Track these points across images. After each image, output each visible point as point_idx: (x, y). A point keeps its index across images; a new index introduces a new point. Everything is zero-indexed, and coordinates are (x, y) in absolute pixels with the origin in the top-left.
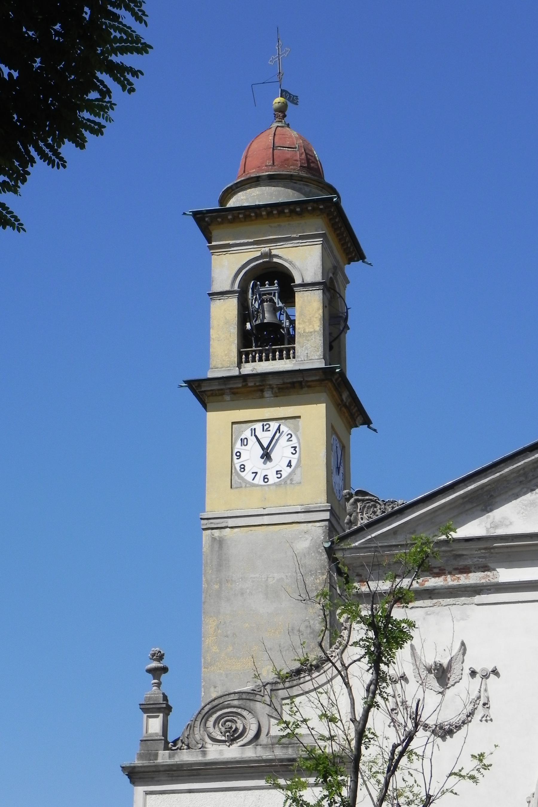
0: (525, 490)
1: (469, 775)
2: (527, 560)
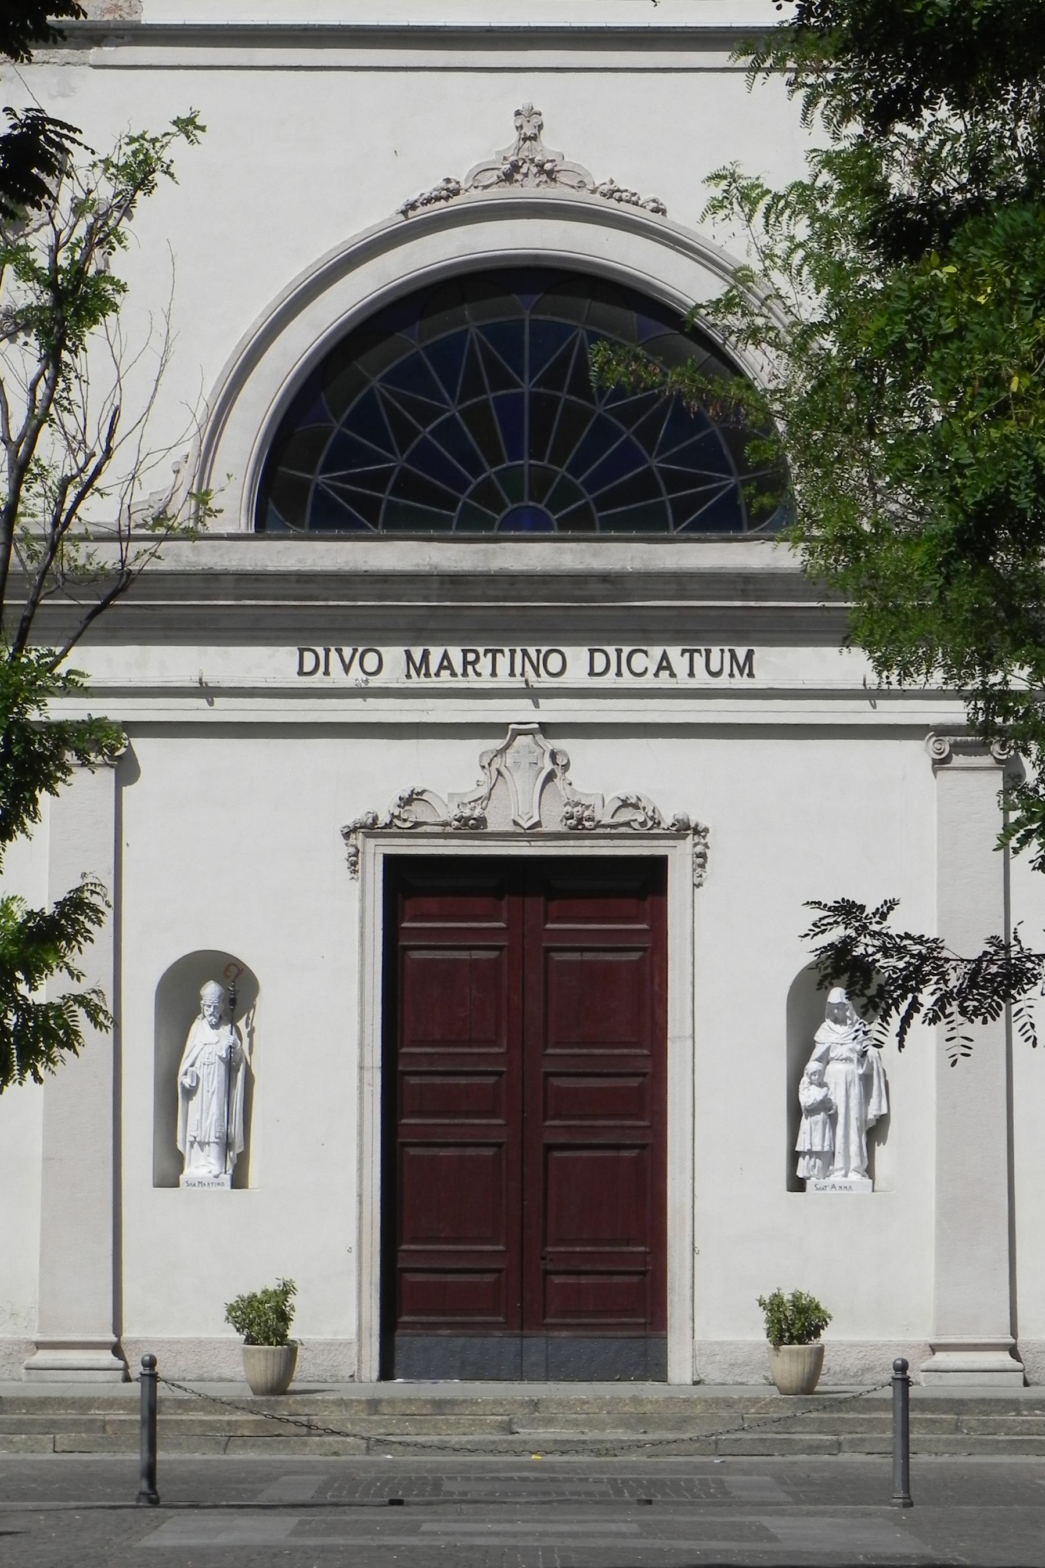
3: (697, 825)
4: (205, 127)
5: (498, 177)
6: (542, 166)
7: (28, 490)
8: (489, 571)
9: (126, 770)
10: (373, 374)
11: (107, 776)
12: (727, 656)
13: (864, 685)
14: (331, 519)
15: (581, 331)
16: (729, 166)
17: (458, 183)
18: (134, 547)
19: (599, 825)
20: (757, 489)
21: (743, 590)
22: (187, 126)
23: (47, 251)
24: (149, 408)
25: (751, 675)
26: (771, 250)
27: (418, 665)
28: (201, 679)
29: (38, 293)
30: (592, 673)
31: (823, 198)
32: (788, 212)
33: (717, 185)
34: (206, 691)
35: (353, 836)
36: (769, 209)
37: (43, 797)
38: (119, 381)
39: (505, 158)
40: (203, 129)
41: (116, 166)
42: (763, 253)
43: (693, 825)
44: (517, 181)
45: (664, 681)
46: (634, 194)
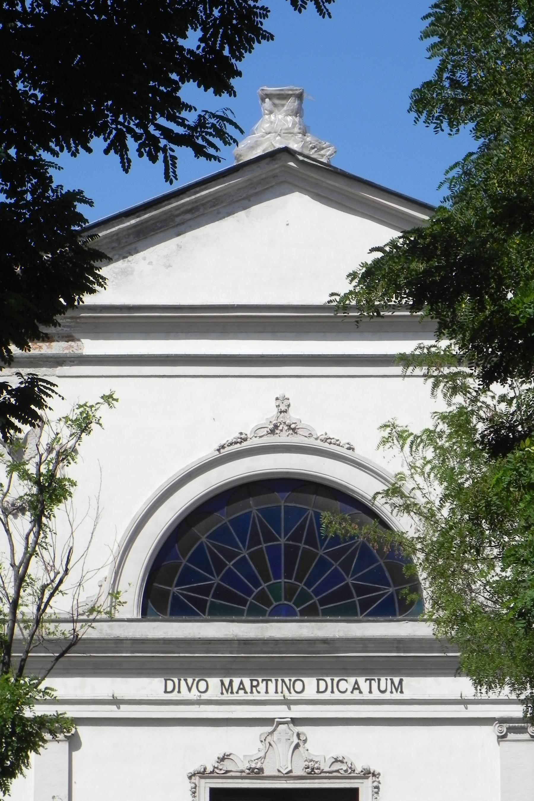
0: (117, 256)
1: (105, 611)
2: (115, 333)
3: (374, 772)
4: (118, 399)
5: (267, 432)
6: (290, 426)
7: (24, 591)
8: (264, 638)
9: (74, 743)
10: (203, 535)
11: (65, 746)
12: (389, 682)
13: (461, 697)
14: (181, 611)
15: (311, 511)
16: (391, 420)
17: (246, 435)
18: (79, 625)
19: (322, 772)
20: (410, 590)
21: (397, 647)
22: (109, 399)
23: (35, 465)
24: (88, 548)
25: (402, 692)
26: (414, 464)
27: (227, 687)
28: (113, 695)
29: (30, 487)
30: (318, 692)
31: (440, 437)
32: (422, 445)
33: (384, 431)
34: (116, 702)
35: (193, 778)
36: (412, 443)
37: (32, 755)
38: (72, 533)
39: (271, 422)
40: (117, 400)
41: (71, 420)
42: (410, 465)
43: (372, 771)
44: (277, 433)
45: (356, 695)
46: (338, 440)
